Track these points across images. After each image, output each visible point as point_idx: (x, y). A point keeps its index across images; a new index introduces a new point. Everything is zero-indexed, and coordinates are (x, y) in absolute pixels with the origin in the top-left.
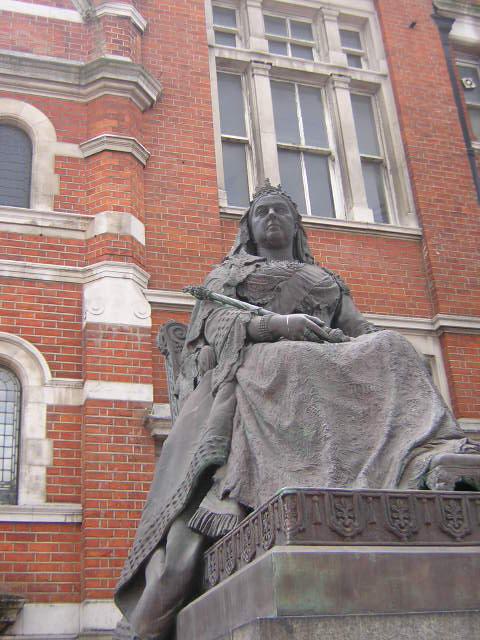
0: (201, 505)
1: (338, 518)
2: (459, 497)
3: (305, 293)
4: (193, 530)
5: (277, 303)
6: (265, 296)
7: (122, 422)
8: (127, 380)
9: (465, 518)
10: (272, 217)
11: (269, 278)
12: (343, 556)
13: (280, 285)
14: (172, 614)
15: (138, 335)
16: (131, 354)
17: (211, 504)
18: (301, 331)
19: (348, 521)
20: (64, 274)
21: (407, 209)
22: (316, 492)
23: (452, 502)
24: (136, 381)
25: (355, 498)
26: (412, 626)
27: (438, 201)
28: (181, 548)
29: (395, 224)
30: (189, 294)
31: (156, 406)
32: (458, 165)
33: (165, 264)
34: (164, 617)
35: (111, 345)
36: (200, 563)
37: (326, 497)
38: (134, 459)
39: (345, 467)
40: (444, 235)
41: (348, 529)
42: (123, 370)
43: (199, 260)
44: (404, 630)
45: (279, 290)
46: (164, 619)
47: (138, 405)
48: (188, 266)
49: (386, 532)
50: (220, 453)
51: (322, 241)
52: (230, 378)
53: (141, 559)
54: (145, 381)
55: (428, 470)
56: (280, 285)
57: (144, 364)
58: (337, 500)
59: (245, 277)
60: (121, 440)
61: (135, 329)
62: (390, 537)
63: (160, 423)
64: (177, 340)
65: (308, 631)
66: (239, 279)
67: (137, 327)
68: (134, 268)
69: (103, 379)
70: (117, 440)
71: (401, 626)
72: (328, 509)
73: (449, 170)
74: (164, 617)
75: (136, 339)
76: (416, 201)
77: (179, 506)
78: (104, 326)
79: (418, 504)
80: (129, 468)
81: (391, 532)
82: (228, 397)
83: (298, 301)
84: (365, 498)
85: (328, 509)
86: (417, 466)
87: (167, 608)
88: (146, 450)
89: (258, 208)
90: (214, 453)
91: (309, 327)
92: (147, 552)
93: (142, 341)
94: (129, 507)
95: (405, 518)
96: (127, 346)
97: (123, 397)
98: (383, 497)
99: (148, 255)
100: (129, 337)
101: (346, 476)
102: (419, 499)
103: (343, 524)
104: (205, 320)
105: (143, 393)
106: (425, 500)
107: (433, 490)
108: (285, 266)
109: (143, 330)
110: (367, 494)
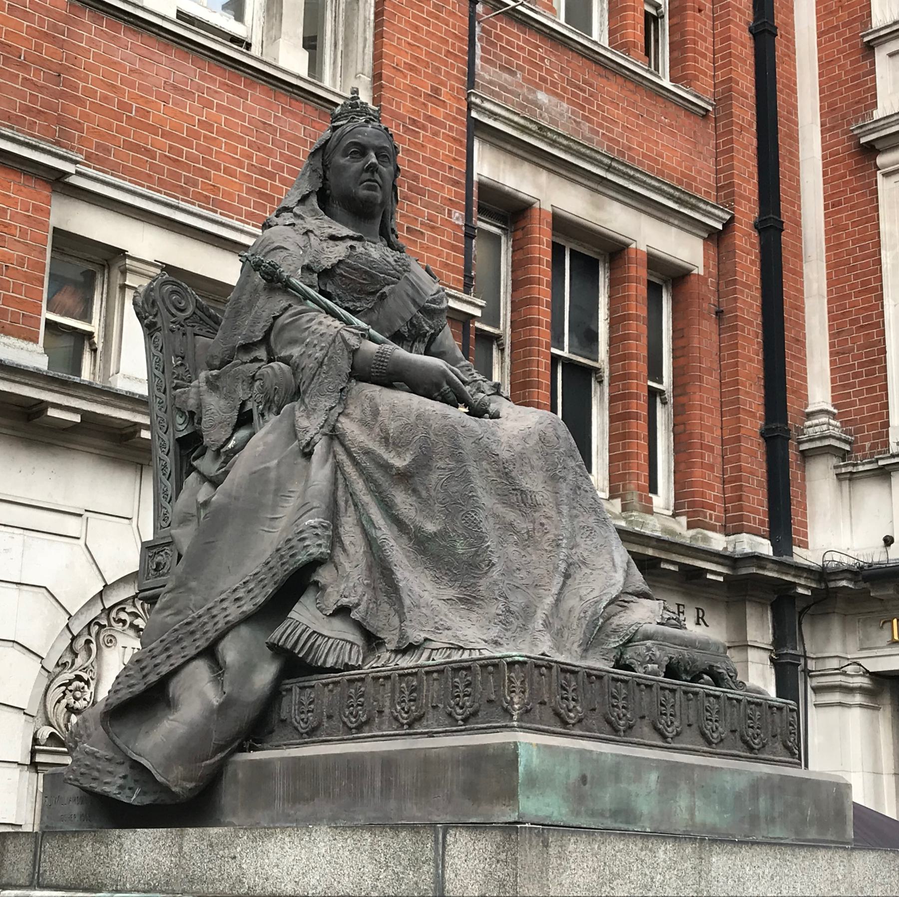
0: (292, 614)
1: (562, 698)
2: (675, 687)
3: (414, 310)
4: (272, 646)
5: (374, 317)
9: (678, 714)
11: (372, 276)
12: (582, 752)
13: (386, 289)
14: (222, 759)
17: (305, 614)
18: (438, 386)
22: (545, 663)
23: (667, 692)
25: (580, 677)
26: (650, 851)
27: (411, 68)
28: (248, 668)
34: (212, 761)
37: (554, 670)
39: (513, 608)
41: (572, 715)
43: (23, 66)
44: (644, 853)
45: (383, 297)
46: (210, 765)
49: (603, 720)
50: (326, 547)
51: (223, 85)
52: (326, 430)
56: (386, 289)
58: (562, 676)
59: (335, 261)
62: (608, 728)
65: (561, 847)
66: (327, 264)
71: (642, 850)
72: (554, 685)
73: (437, 18)
76: (378, 57)
77: (248, 607)
81: (610, 723)
82: (327, 461)
83: (403, 319)
84: (589, 675)
86: (615, 631)
87: (220, 749)
91: (450, 382)
92: (177, 661)
95: (623, 707)
98: (606, 678)
102: (638, 684)
103: (567, 706)
106: (643, 687)
108: (391, 260)
110: (592, 672)
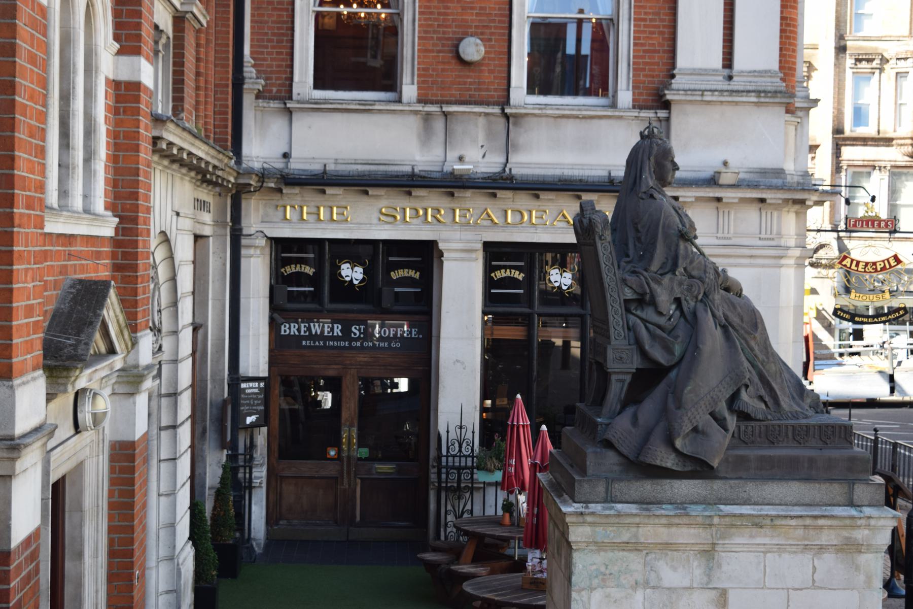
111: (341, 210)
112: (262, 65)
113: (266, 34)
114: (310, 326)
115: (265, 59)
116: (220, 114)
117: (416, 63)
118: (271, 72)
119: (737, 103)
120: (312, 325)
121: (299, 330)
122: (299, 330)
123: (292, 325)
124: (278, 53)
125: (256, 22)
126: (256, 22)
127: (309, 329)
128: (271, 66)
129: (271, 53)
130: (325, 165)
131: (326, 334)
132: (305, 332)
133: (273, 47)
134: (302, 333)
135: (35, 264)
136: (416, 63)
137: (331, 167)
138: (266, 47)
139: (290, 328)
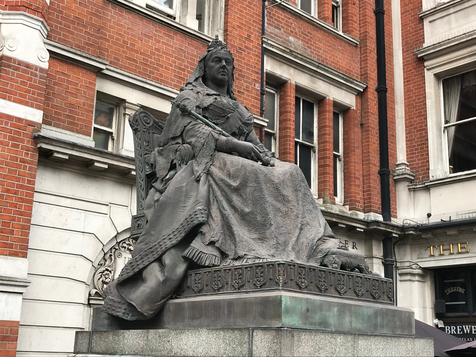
0: (192, 245)
3: (240, 123)
4: (184, 257)
5: (225, 126)
6: (218, 119)
7: (19, 133)
8: (26, 104)
10: (224, 67)
11: (223, 110)
12: (307, 299)
13: (229, 115)
15: (38, 73)
16: (31, 86)
17: (197, 244)
18: (250, 154)
19: (303, 280)
20: (7, 17)
21: (219, 28)
24: (32, 106)
28: (174, 266)
29: (208, 33)
30: (46, 33)
31: (43, 126)
32: (255, 5)
33: (61, 23)
34: (160, 303)
35: (19, 76)
36: (185, 276)
37: (296, 267)
38: (23, 161)
39: (280, 242)
40: (237, 52)
41: (303, 284)
42: (24, 96)
43: (85, 26)
45: (228, 118)
47: (31, 124)
48: (76, 29)
49: (315, 287)
51: (164, 34)
53: (141, 266)
54: (38, 108)
55: (326, 255)
56: (229, 115)
57: (39, 95)
58: (299, 269)
59: (209, 104)
60: (17, 146)
61: (36, 68)
62: (317, 290)
63: (43, 140)
64: (145, 124)
66: (206, 105)
67: (38, 66)
68: (42, 23)
69: (10, 100)
70: (13, 145)
73: (250, 7)
74: (160, 303)
75: (36, 76)
77: (174, 242)
78: (15, 60)
79: (329, 274)
80: (19, 166)
83: (236, 127)
85: (296, 273)
86: (320, 251)
87: (163, 298)
88: (32, 156)
89: (217, 57)
90: (203, 217)
91: (255, 152)
92: (146, 263)
93: (40, 78)
94: (15, 194)
96: (30, 79)
97: (22, 116)
98: (317, 270)
99: (50, 13)
100: (32, 73)
101: (281, 248)
104: (185, 127)
105: (35, 115)
107: (330, 268)
109: (42, 70)
111: (463, 246)
112: (413, 165)
113: (414, 146)
114: (463, 327)
115: (415, 161)
116: (366, 192)
117: (261, 118)
118: (419, 167)
119: (314, 77)
120: (464, 326)
121: (456, 330)
122: (456, 330)
123: (452, 327)
124: (421, 155)
125: (409, 141)
126: (409, 141)
127: (462, 329)
128: (418, 164)
129: (418, 156)
130: (450, 217)
131: (473, 333)
132: (460, 332)
133: (418, 153)
134: (459, 333)
135: (8, 236)
136: (261, 118)
137: (454, 218)
138: (415, 153)
139: (450, 329)
